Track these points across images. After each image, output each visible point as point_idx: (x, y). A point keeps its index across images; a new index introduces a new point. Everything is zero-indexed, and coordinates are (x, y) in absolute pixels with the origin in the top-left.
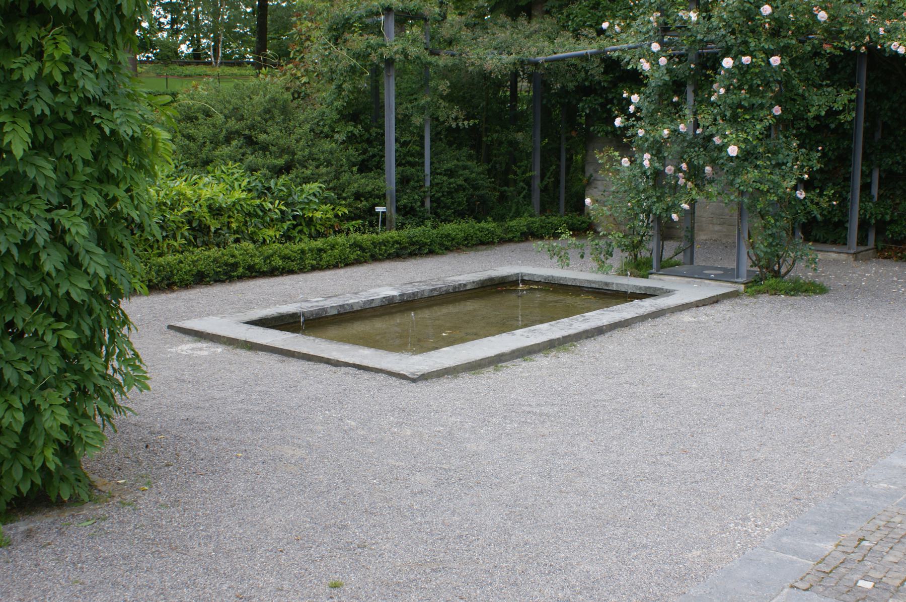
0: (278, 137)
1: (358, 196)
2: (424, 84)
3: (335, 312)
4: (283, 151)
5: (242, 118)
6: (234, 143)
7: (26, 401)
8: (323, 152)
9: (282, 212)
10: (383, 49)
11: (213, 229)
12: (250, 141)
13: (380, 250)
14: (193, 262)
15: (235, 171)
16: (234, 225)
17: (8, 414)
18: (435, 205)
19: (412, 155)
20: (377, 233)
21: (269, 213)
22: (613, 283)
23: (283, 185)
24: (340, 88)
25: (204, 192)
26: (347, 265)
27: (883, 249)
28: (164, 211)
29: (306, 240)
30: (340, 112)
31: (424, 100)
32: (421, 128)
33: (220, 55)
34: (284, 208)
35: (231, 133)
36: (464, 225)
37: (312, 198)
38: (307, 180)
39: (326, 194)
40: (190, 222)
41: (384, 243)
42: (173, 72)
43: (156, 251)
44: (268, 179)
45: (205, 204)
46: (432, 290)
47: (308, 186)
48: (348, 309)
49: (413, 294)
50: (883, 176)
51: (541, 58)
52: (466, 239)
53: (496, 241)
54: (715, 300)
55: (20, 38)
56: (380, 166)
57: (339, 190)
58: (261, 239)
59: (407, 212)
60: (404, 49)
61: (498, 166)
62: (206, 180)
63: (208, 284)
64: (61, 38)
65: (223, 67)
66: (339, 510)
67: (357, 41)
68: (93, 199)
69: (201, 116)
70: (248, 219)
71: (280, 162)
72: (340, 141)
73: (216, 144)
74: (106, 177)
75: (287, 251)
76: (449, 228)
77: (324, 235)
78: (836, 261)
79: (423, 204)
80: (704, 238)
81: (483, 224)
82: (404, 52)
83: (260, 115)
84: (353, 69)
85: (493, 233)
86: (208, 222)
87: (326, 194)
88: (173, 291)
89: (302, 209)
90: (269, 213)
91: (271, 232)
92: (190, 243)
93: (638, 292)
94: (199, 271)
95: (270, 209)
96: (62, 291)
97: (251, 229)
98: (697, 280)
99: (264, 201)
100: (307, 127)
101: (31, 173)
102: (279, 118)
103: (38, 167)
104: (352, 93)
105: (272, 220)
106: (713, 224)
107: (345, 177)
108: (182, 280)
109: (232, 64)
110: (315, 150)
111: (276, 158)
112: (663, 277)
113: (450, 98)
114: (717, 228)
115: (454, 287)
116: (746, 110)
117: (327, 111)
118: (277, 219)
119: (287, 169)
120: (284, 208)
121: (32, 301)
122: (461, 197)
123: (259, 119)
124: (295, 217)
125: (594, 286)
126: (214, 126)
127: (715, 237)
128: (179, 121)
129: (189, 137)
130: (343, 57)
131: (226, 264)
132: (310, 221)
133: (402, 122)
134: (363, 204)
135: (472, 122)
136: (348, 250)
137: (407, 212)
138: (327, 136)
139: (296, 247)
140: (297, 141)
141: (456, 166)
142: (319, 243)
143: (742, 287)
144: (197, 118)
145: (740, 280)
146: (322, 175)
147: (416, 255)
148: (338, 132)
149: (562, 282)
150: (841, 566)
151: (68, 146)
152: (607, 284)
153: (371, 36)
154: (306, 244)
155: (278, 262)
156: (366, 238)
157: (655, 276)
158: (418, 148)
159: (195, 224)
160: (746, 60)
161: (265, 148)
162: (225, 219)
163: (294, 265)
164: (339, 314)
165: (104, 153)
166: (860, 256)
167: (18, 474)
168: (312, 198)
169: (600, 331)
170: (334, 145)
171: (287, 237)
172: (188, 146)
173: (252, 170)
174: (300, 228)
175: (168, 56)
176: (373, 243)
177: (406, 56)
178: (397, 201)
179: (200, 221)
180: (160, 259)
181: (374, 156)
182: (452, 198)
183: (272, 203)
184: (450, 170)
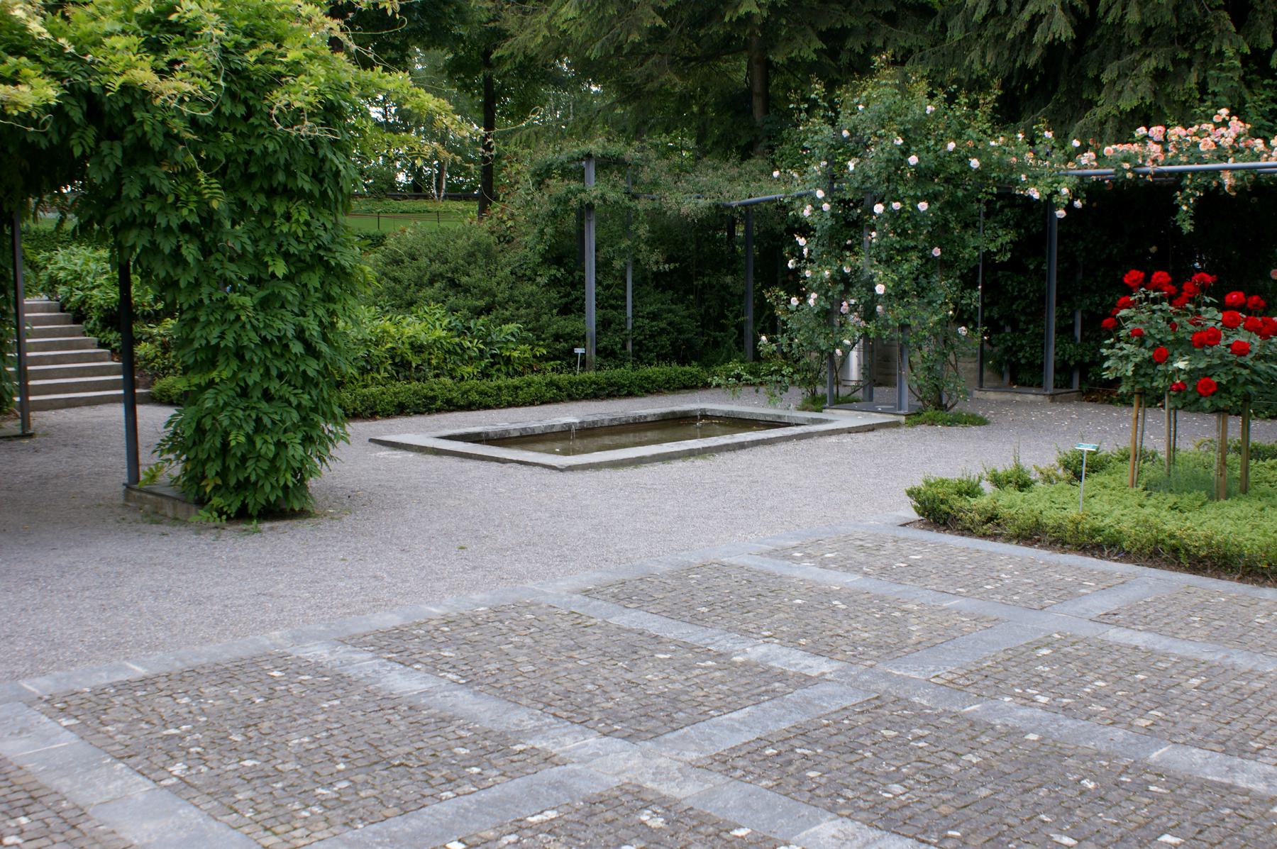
0: (480, 280)
1: (557, 337)
2: (626, 231)
3: (518, 434)
4: (485, 293)
5: (446, 262)
6: (437, 285)
7: (275, 439)
8: (524, 295)
9: (481, 351)
10: (583, 195)
11: (414, 365)
12: (453, 284)
13: (577, 389)
14: (395, 393)
15: (437, 311)
16: (434, 362)
17: (264, 447)
18: (637, 348)
19: (615, 298)
20: (575, 374)
21: (468, 351)
23: (483, 325)
24: (542, 232)
25: (406, 330)
26: (543, 403)
27: (1090, 392)
28: (370, 346)
29: (503, 377)
30: (542, 256)
31: (625, 243)
32: (623, 271)
33: (444, 187)
34: (482, 347)
35: (435, 276)
36: (667, 369)
37: (509, 337)
38: (506, 321)
39: (525, 334)
40: (393, 358)
41: (582, 383)
42: (388, 207)
43: (361, 384)
44: (468, 320)
45: (407, 341)
46: (611, 420)
47: (507, 326)
48: (530, 432)
49: (593, 422)
50: (1086, 317)
51: (735, 203)
52: (668, 382)
53: (700, 385)
54: (871, 428)
55: (276, 208)
56: (582, 309)
57: (538, 331)
58: (459, 375)
59: (606, 354)
60: (603, 194)
61: (711, 311)
62: (409, 320)
63: (408, 415)
64: (302, 208)
65: (446, 202)
67: (557, 186)
68: (321, 312)
69: (406, 259)
70: (447, 356)
71: (481, 303)
72: (542, 283)
73: (420, 285)
74: (329, 298)
75: (483, 387)
76: (649, 371)
77: (521, 374)
79: (624, 347)
81: (687, 368)
82: (603, 198)
83: (463, 259)
84: (554, 215)
85: (696, 377)
86: (410, 358)
87: (525, 334)
88: (376, 420)
89: (499, 348)
90: (468, 351)
91: (469, 369)
92: (392, 377)
94: (400, 403)
95: (469, 348)
96: (301, 369)
97: (450, 366)
99: (464, 339)
100: (508, 270)
101: (284, 293)
102: (482, 262)
103: (287, 289)
104: (554, 237)
105: (471, 358)
107: (545, 318)
108: (384, 410)
109: (458, 198)
110: (516, 293)
111: (477, 299)
112: (835, 411)
113: (652, 243)
115: (635, 419)
116: (899, 252)
117: (530, 255)
118: (475, 357)
119: (488, 310)
120: (482, 347)
121: (281, 376)
122: (664, 340)
123: (461, 262)
124: (493, 356)
125: (768, 419)
126: (419, 268)
128: (386, 264)
129: (395, 280)
130: (543, 203)
131: (426, 397)
132: (508, 360)
133: (603, 266)
134: (562, 345)
135: (672, 266)
136: (544, 388)
137: (606, 354)
138: (530, 279)
139: (493, 384)
140: (498, 284)
141: (659, 310)
142: (516, 381)
143: (903, 419)
144: (402, 262)
145: (902, 412)
146: (522, 316)
147: (614, 396)
148: (540, 275)
151: (304, 278)
152: (779, 417)
153: (572, 182)
154: (503, 381)
155: (474, 397)
156: (563, 378)
158: (621, 292)
159: (397, 361)
160: (896, 206)
161: (467, 290)
162: (425, 356)
163: (490, 401)
164: (521, 436)
165: (327, 283)
166: (1058, 398)
167: (268, 488)
168: (509, 337)
169: (741, 446)
170: (534, 287)
171: (485, 374)
172: (393, 288)
173: (453, 310)
174: (498, 366)
175: (382, 189)
176: (569, 383)
177: (605, 201)
178: (597, 343)
179: (403, 357)
180: (365, 391)
181: (577, 299)
182: (655, 341)
183: (471, 342)
184: (653, 313)
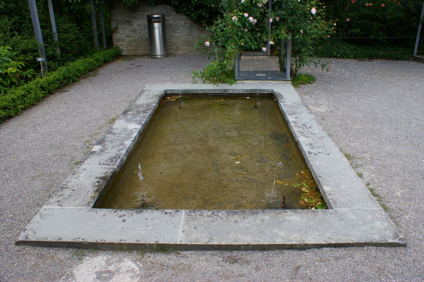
22: (230, 90)
78: (263, 59)
80: (181, 53)
93: (246, 93)
98: (264, 81)
114: (186, 48)
125: (217, 92)
127: (186, 52)
142: (20, 91)
149: (194, 92)
150: (283, 200)
152: (225, 90)
157: (239, 81)
178: (46, 53)
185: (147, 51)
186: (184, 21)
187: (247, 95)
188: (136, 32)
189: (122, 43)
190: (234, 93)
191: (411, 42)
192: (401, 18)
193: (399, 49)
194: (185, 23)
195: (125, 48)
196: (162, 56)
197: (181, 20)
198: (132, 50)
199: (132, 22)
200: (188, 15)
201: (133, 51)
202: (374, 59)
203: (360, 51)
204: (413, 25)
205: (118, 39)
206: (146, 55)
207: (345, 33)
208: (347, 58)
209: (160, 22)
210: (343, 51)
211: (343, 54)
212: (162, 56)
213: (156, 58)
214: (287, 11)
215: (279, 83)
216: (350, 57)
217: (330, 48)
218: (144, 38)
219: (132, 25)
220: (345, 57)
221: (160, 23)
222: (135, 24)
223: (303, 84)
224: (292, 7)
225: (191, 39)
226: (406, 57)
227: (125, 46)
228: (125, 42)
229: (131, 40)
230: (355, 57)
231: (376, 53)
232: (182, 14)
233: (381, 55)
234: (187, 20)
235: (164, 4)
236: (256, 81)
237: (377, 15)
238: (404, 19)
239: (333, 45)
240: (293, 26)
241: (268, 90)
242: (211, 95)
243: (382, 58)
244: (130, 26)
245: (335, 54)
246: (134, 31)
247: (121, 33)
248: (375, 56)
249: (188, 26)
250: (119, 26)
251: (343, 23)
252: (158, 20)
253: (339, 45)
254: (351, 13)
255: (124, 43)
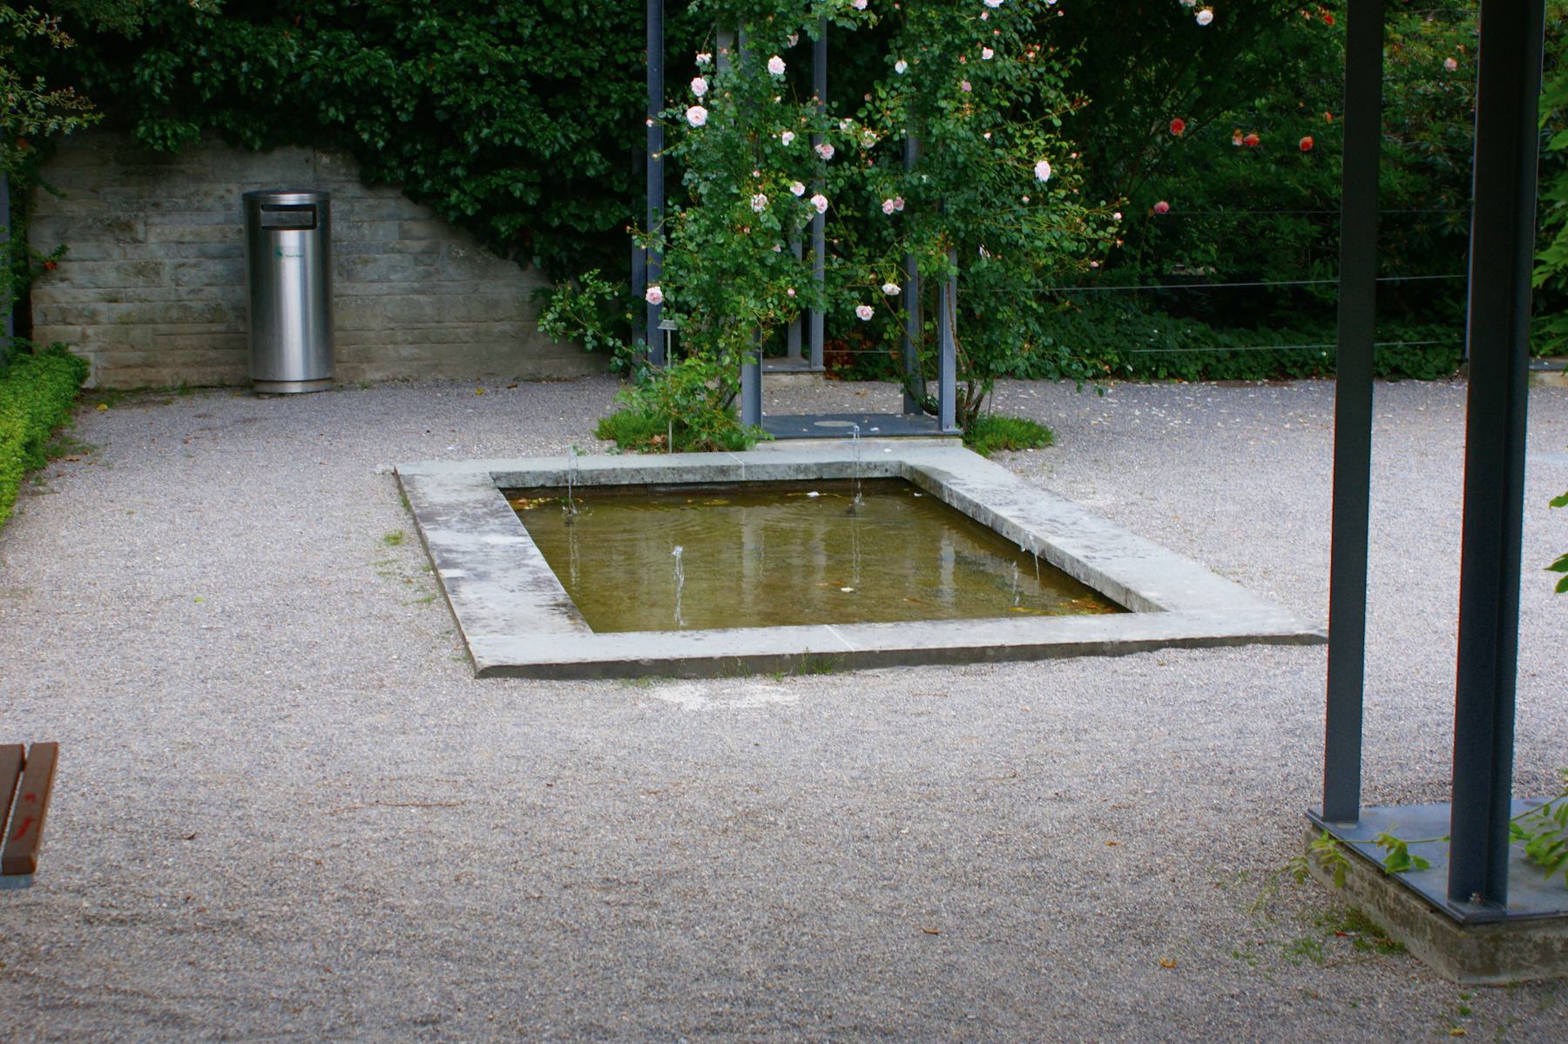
22: (739, 467)
66: (535, 886)
93: (801, 477)
106: (395, 343)
114: (406, 351)
149: (603, 481)
185: (209, 370)
186: (400, 226)
187: (808, 485)
188: (158, 274)
189: (79, 329)
190: (755, 478)
191: (1449, 301)
192: (1396, 193)
193: (1400, 332)
194: (404, 235)
195: (92, 357)
196: (311, 387)
197: (382, 219)
198: (129, 366)
199: (140, 227)
200: (415, 197)
201: (137, 371)
202: (1294, 377)
203: (1226, 346)
204: (1447, 224)
205: (63, 311)
206: (203, 387)
207: (1154, 267)
208: (1171, 376)
209: (313, 227)
210: (1150, 346)
211: (1152, 358)
212: (311, 387)
213: (282, 395)
214: (941, 173)
215: (916, 446)
216: (1184, 371)
217: (1088, 337)
218: (197, 305)
219: (135, 241)
220: (1162, 373)
221: (309, 233)
222: (152, 239)
223: (1007, 447)
224: (961, 159)
225: (429, 310)
226: (1437, 362)
227: (93, 346)
228: (95, 323)
229: (129, 315)
230: (1206, 375)
231: (1300, 353)
232: (390, 193)
233: (1322, 358)
234: (414, 219)
235: (301, 145)
236: (826, 442)
237: (1291, 181)
238: (1406, 197)
239: (1100, 321)
240: (966, 227)
241: (882, 465)
242: (663, 489)
243: (1328, 371)
244: (129, 248)
245: (1116, 359)
246: (147, 271)
247: (79, 279)
248: (1295, 364)
249: (417, 246)
250: (74, 249)
251: (1142, 223)
252: (297, 218)
253: (1127, 321)
254: (1171, 179)
255: (90, 331)
